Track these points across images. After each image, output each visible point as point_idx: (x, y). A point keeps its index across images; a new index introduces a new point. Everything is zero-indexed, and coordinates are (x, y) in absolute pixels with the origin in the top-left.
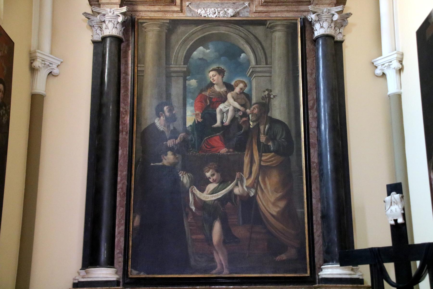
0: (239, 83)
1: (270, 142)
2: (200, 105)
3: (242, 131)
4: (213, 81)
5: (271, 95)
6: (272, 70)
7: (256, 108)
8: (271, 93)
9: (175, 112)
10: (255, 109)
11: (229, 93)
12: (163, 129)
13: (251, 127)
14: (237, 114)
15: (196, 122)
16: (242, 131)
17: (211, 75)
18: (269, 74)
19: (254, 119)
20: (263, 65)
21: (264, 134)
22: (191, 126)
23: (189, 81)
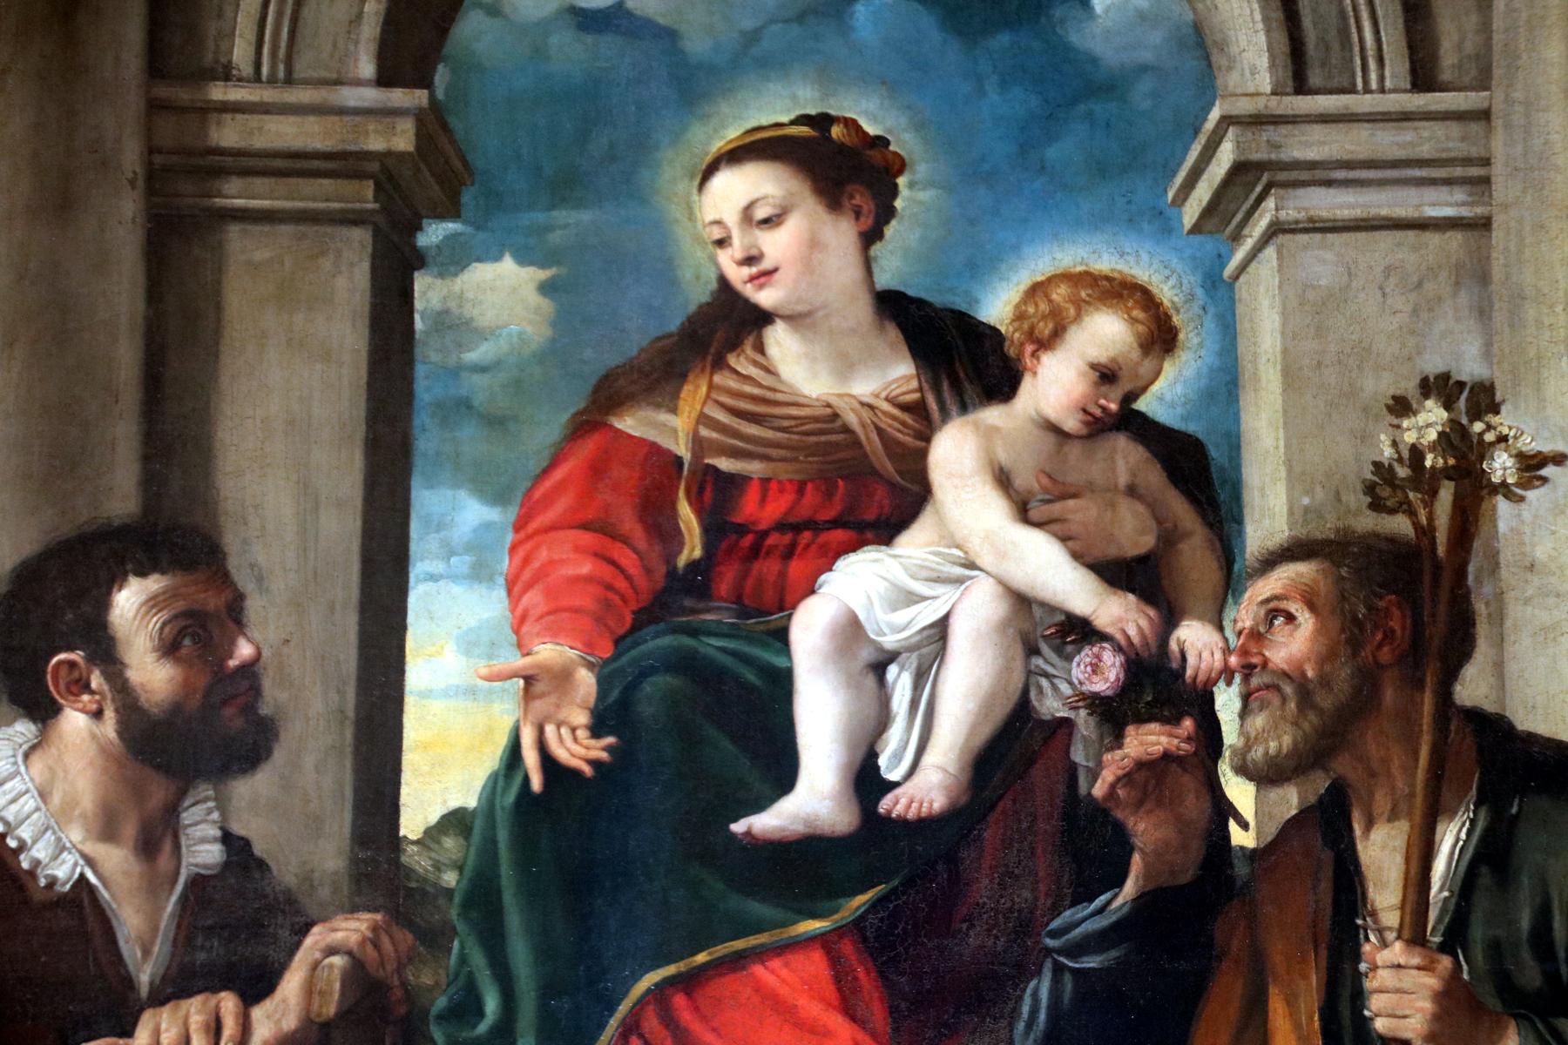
0: (1081, 307)
1: (1506, 1028)
2: (586, 568)
3: (1130, 889)
4: (752, 279)
5: (1483, 450)
6: (1499, 146)
7: (1294, 607)
8: (1494, 420)
9: (258, 656)
10: (1290, 618)
11: (946, 416)
12: (90, 861)
13: (1241, 838)
14: (1047, 675)
15: (526, 780)
16: (1130, 889)
17: (732, 218)
18: (1459, 195)
19: (1282, 742)
20: (1382, 90)
21: (1415, 937)
22: (456, 821)
23: (441, 275)
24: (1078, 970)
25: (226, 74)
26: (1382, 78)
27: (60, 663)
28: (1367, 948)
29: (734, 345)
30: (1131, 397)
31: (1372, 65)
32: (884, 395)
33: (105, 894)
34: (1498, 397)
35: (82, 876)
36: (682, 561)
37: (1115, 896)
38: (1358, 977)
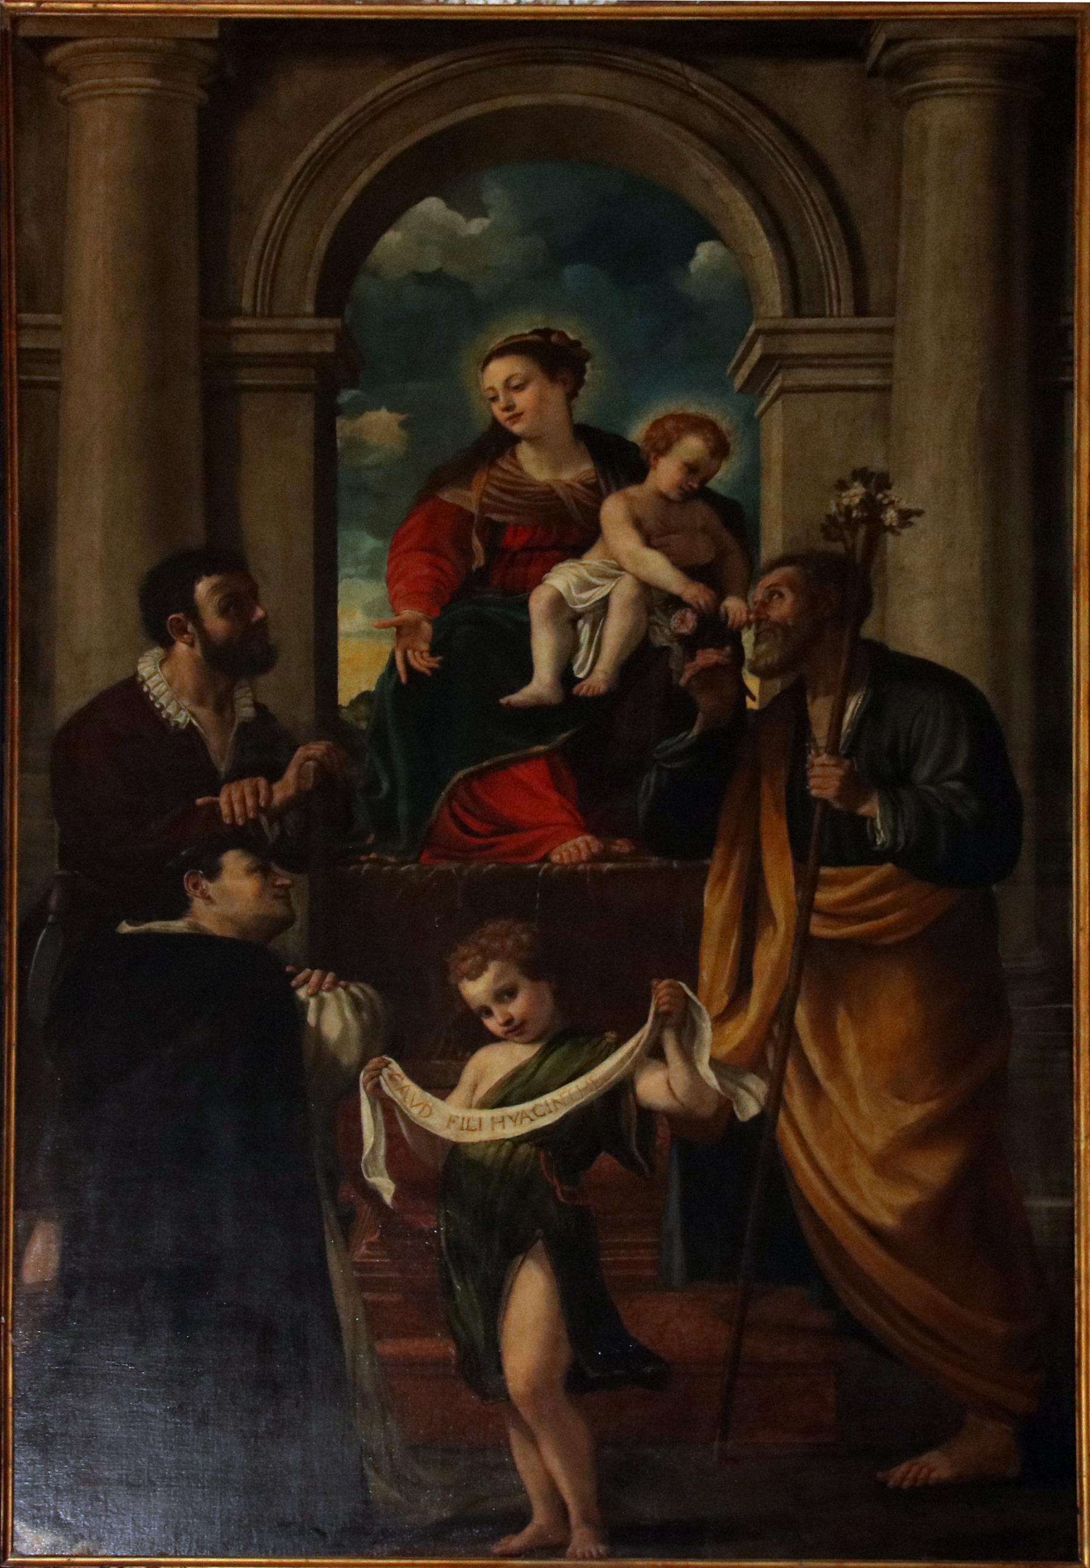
2: (426, 571)
3: (696, 730)
4: (509, 418)
7: (784, 590)
8: (889, 492)
9: (265, 617)
10: (781, 595)
11: (609, 492)
12: (193, 715)
13: (752, 705)
15: (399, 678)
16: (696, 730)
17: (498, 384)
18: (877, 372)
20: (839, 316)
21: (833, 750)
22: (364, 697)
24: (670, 769)
25: (239, 313)
26: (839, 310)
27: (172, 619)
28: (810, 757)
29: (500, 454)
30: (706, 480)
31: (835, 302)
32: (577, 479)
33: (202, 731)
34: (891, 480)
35: (190, 722)
36: (474, 567)
37: (689, 734)
38: (805, 771)
